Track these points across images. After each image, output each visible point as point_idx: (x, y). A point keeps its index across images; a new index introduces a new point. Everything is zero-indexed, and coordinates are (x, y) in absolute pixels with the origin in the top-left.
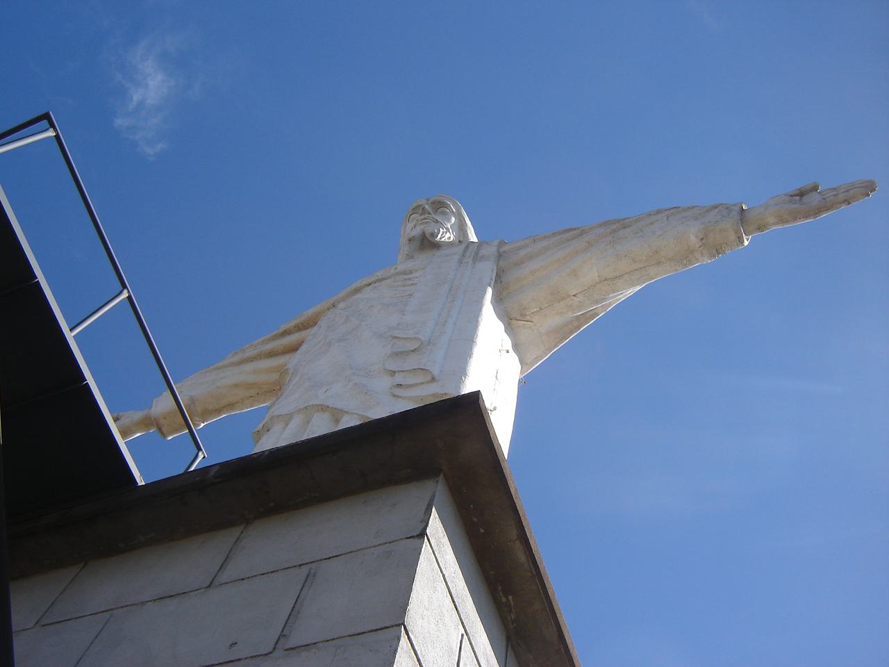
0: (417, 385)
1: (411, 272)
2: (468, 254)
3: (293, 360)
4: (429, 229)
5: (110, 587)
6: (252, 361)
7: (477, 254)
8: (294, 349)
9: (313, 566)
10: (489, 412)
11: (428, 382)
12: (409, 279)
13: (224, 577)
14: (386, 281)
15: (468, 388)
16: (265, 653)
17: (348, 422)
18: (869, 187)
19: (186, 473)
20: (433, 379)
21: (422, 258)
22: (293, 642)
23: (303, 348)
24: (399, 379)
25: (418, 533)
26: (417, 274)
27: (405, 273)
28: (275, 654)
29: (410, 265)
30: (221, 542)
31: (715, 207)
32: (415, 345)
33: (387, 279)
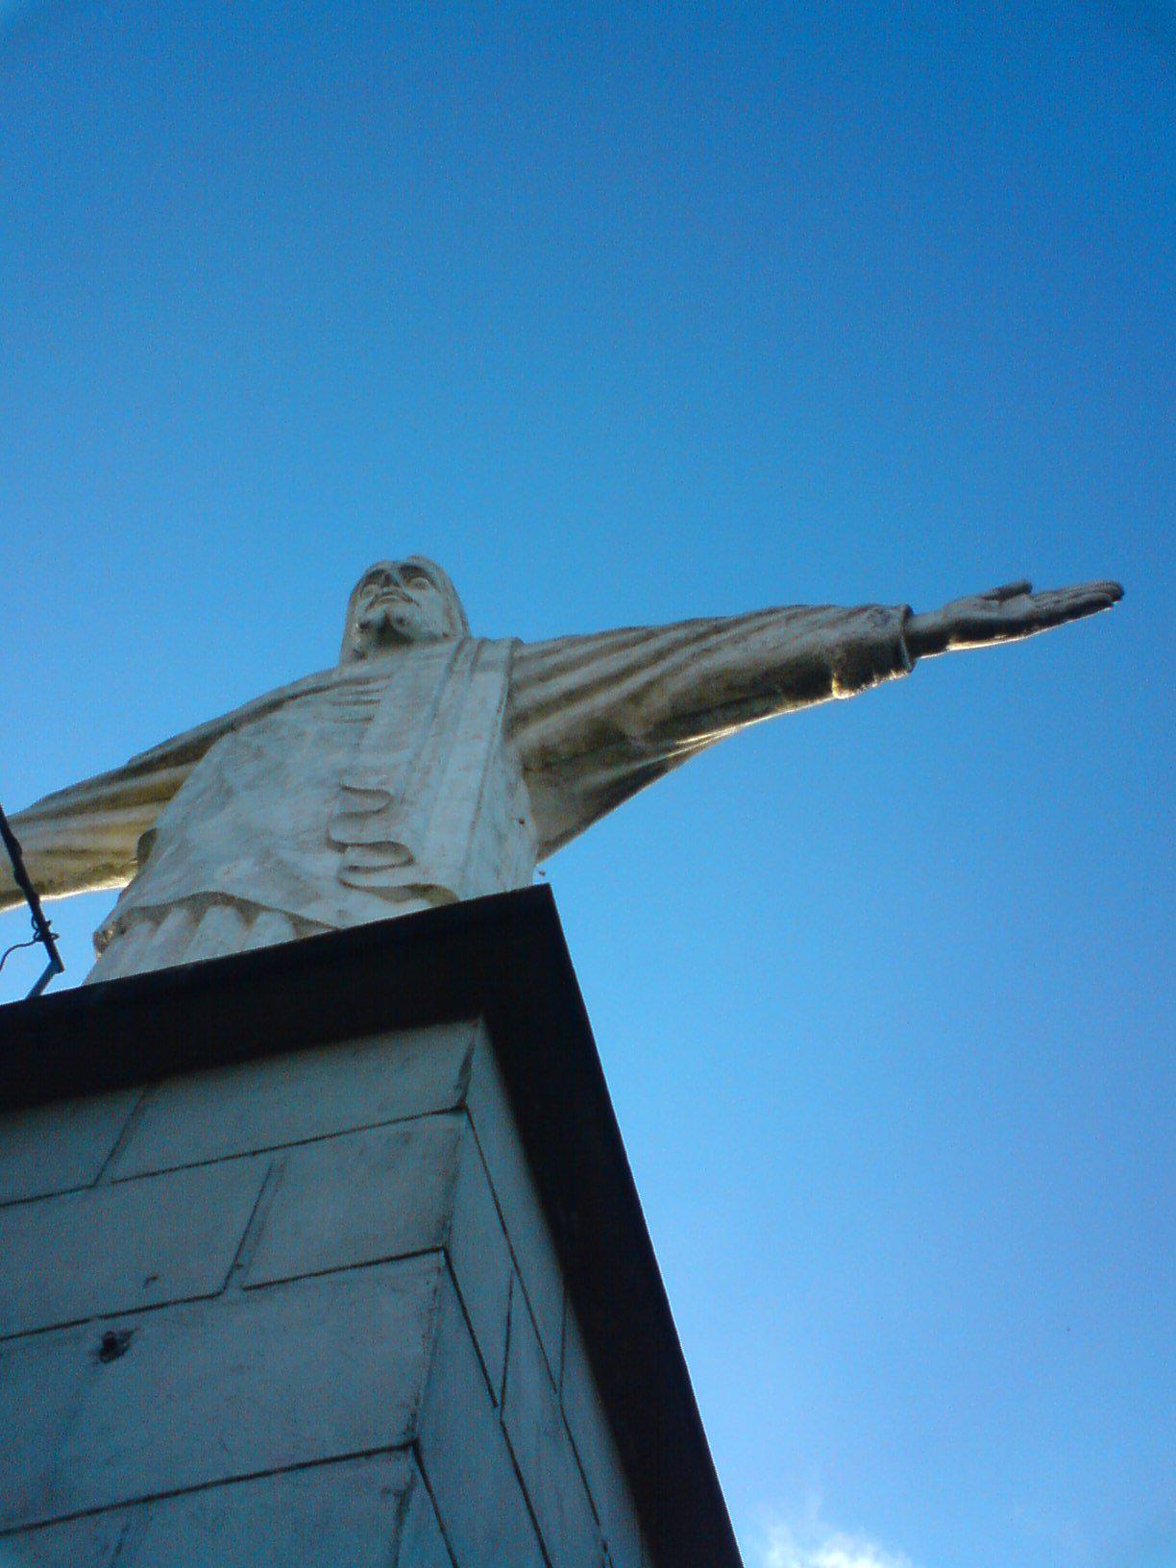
1: (366, 681)
3: (164, 817)
4: (400, 610)
6: (81, 812)
8: (163, 795)
9: (278, 1155)
12: (366, 693)
13: (120, 1170)
15: (537, 880)
16: (210, 1292)
18: (1117, 594)
19: (35, 1000)
20: (410, 861)
21: (383, 662)
22: (257, 1275)
23: (182, 796)
24: (353, 856)
27: (358, 681)
31: (864, 609)
32: (378, 804)
33: (328, 688)
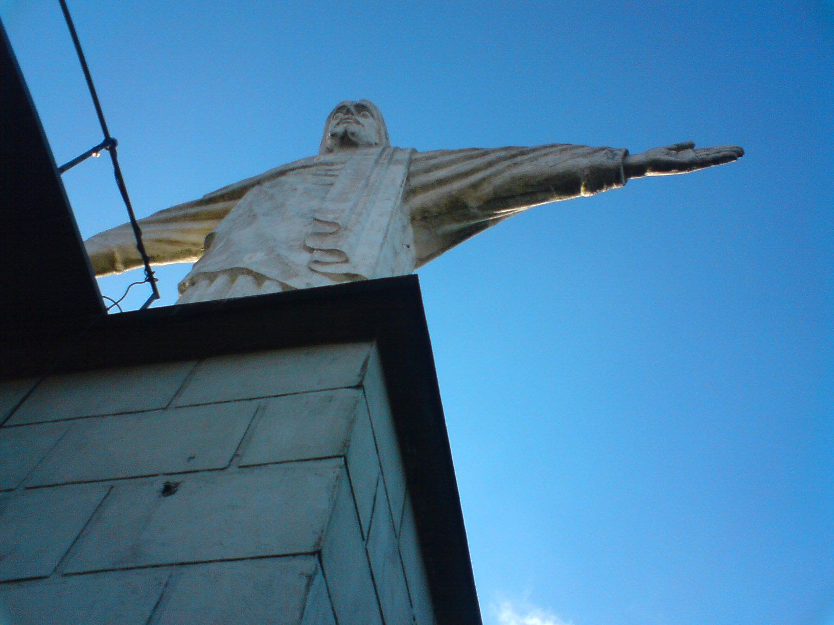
0: (333, 263)
1: (332, 164)
2: (384, 157)
3: (220, 227)
4: (353, 128)
5: (67, 401)
7: (392, 155)
8: (220, 216)
9: (263, 401)
10: (155, 304)
11: (342, 262)
14: (311, 169)
17: (270, 288)
20: (347, 261)
21: (341, 155)
22: (245, 461)
23: (229, 217)
24: (317, 255)
25: (356, 384)
26: (338, 167)
27: (327, 164)
28: (230, 470)
29: (330, 158)
30: (178, 373)
31: (603, 149)
32: (333, 229)
